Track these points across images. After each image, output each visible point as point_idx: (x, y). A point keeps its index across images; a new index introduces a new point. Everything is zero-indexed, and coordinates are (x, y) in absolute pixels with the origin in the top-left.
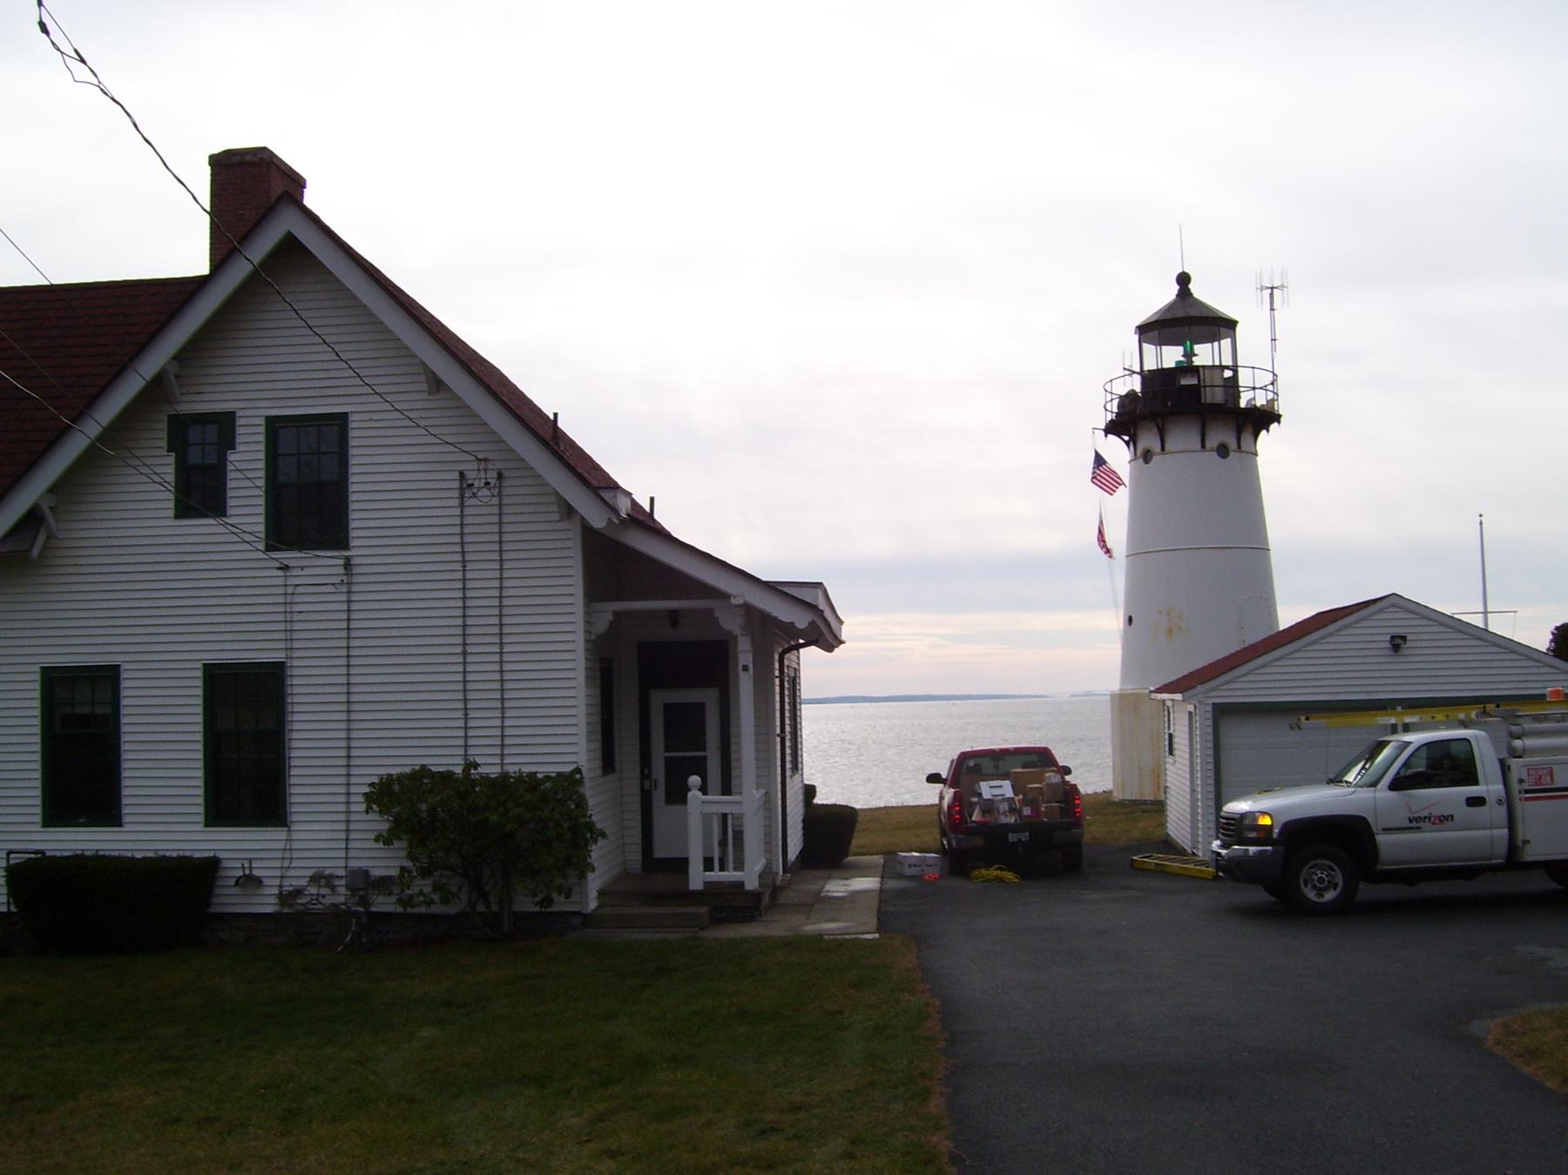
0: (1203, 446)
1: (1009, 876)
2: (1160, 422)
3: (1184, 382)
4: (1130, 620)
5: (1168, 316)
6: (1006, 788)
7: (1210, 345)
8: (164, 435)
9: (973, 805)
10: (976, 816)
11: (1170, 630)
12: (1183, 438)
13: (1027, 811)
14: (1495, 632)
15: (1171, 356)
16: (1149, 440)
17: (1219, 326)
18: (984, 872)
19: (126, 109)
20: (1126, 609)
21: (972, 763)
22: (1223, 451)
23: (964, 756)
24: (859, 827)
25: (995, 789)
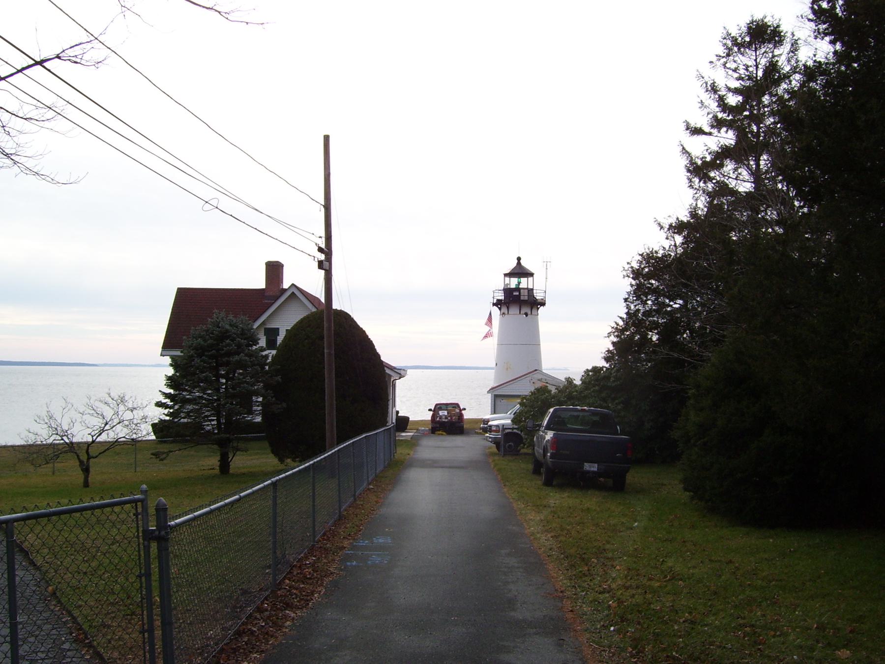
0: (520, 313)
1: (444, 433)
2: (507, 305)
3: (515, 294)
4: (496, 364)
5: (513, 272)
6: (446, 413)
7: (526, 279)
8: (263, 332)
9: (437, 417)
10: (438, 419)
11: (507, 369)
12: (514, 310)
13: (449, 418)
14: (451, 402)
15: (513, 282)
16: (504, 310)
17: (528, 274)
18: (438, 432)
19: (114, 130)
20: (496, 361)
21: (439, 406)
22: (526, 314)
23: (437, 405)
24: (409, 424)
25: (443, 413)
